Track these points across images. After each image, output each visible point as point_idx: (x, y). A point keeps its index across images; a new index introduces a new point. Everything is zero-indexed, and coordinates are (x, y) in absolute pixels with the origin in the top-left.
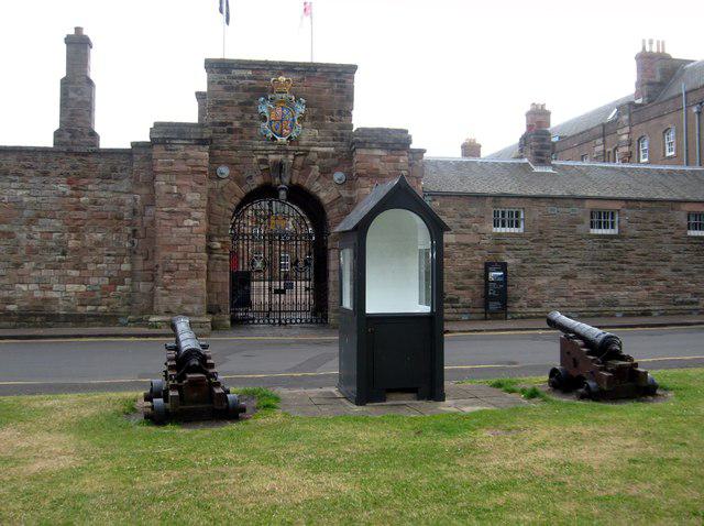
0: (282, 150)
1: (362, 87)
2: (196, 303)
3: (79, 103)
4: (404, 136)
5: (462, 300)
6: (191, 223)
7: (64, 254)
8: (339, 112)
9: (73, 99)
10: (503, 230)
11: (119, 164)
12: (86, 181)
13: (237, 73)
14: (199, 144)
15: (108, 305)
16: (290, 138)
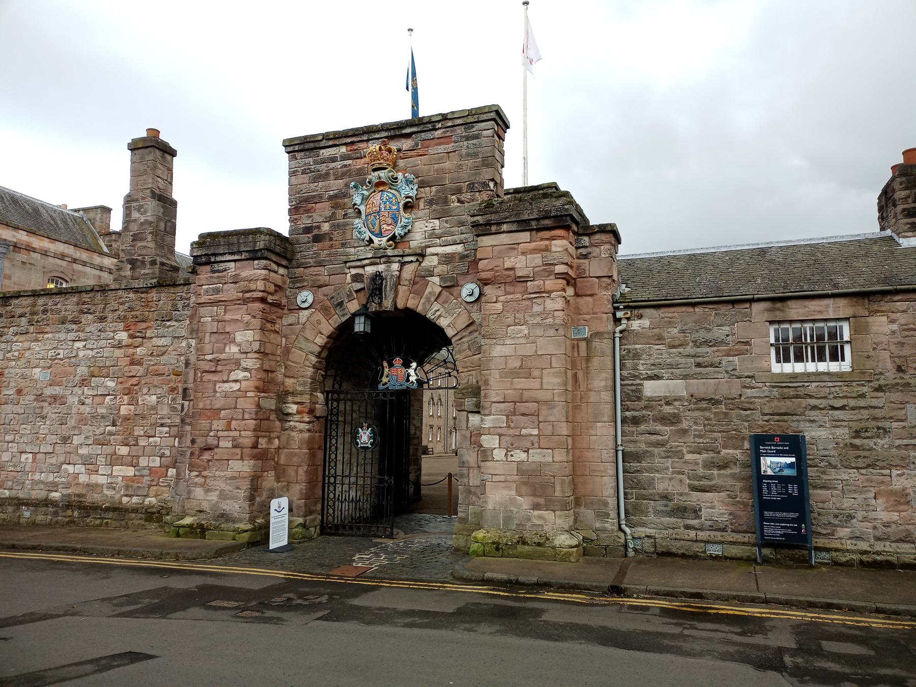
0: (380, 257)
3: (142, 224)
7: (114, 425)
9: (135, 221)
10: (799, 368)
12: (144, 325)
15: (156, 496)
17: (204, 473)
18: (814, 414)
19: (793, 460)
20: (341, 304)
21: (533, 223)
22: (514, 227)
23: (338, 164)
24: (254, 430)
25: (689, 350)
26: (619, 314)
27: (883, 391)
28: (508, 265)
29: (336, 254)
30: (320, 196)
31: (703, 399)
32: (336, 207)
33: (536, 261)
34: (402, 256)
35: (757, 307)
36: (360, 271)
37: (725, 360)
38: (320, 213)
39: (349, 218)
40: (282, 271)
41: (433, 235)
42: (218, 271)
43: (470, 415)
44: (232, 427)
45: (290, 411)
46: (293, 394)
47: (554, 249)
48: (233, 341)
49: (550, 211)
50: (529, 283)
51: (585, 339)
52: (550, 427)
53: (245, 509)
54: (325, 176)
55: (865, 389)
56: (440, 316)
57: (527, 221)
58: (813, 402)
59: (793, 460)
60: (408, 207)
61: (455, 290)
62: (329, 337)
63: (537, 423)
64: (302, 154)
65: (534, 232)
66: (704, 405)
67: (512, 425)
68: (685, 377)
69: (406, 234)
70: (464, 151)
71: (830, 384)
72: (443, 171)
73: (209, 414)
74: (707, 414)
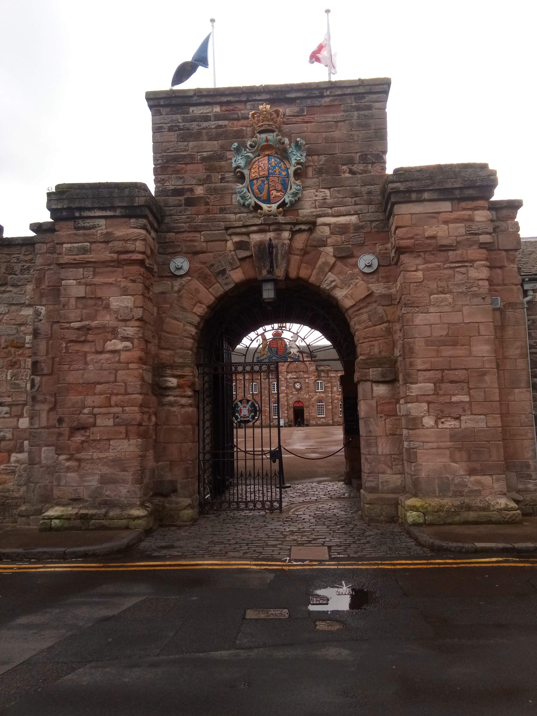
0: (270, 224)
1: (397, 112)
2: (124, 481)
4: (483, 174)
6: (120, 345)
8: (364, 159)
11: (19, 261)
13: (197, 111)
14: (130, 217)
16: (283, 204)
17: (78, 456)
20: (223, 272)
21: (457, 192)
22: (435, 196)
23: (212, 124)
24: (141, 406)
26: (527, 287)
28: (429, 232)
29: (214, 220)
30: (192, 157)
32: (210, 169)
33: (459, 230)
34: (295, 224)
36: (244, 238)
38: (192, 177)
39: (228, 182)
41: (324, 204)
42: (84, 228)
43: (374, 385)
44: (113, 403)
45: (170, 384)
46: (172, 367)
47: (477, 218)
48: (107, 307)
49: (476, 181)
50: (450, 253)
51: (498, 309)
52: (482, 394)
53: (135, 493)
54: (197, 136)
56: (335, 287)
57: (451, 190)
60: (297, 174)
61: (352, 261)
62: (208, 307)
63: (466, 390)
64: (168, 109)
65: (455, 202)
67: (441, 392)
69: (296, 201)
70: (355, 121)
72: (333, 141)
73: (80, 389)
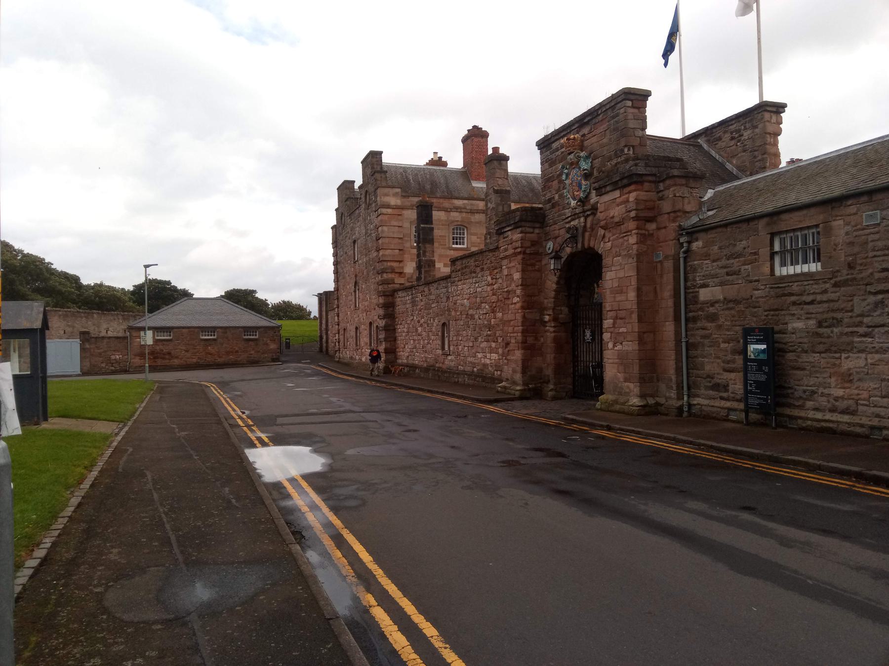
5: (731, 387)
18: (794, 310)
19: (763, 347)
25: (724, 262)
27: (839, 286)
31: (731, 301)
35: (762, 223)
37: (743, 268)
40: (537, 231)
55: (828, 285)
58: (793, 298)
59: (763, 347)
66: (731, 305)
68: (722, 284)
71: (806, 283)
74: (733, 312)
